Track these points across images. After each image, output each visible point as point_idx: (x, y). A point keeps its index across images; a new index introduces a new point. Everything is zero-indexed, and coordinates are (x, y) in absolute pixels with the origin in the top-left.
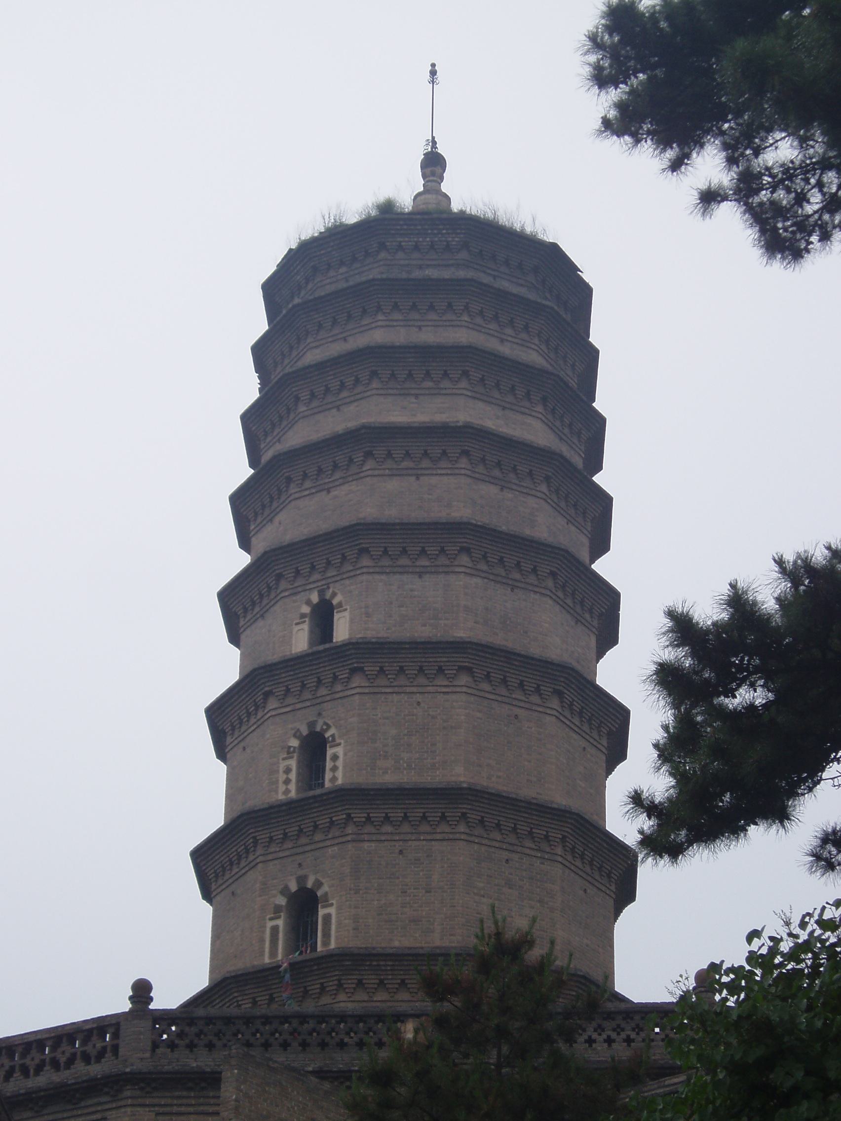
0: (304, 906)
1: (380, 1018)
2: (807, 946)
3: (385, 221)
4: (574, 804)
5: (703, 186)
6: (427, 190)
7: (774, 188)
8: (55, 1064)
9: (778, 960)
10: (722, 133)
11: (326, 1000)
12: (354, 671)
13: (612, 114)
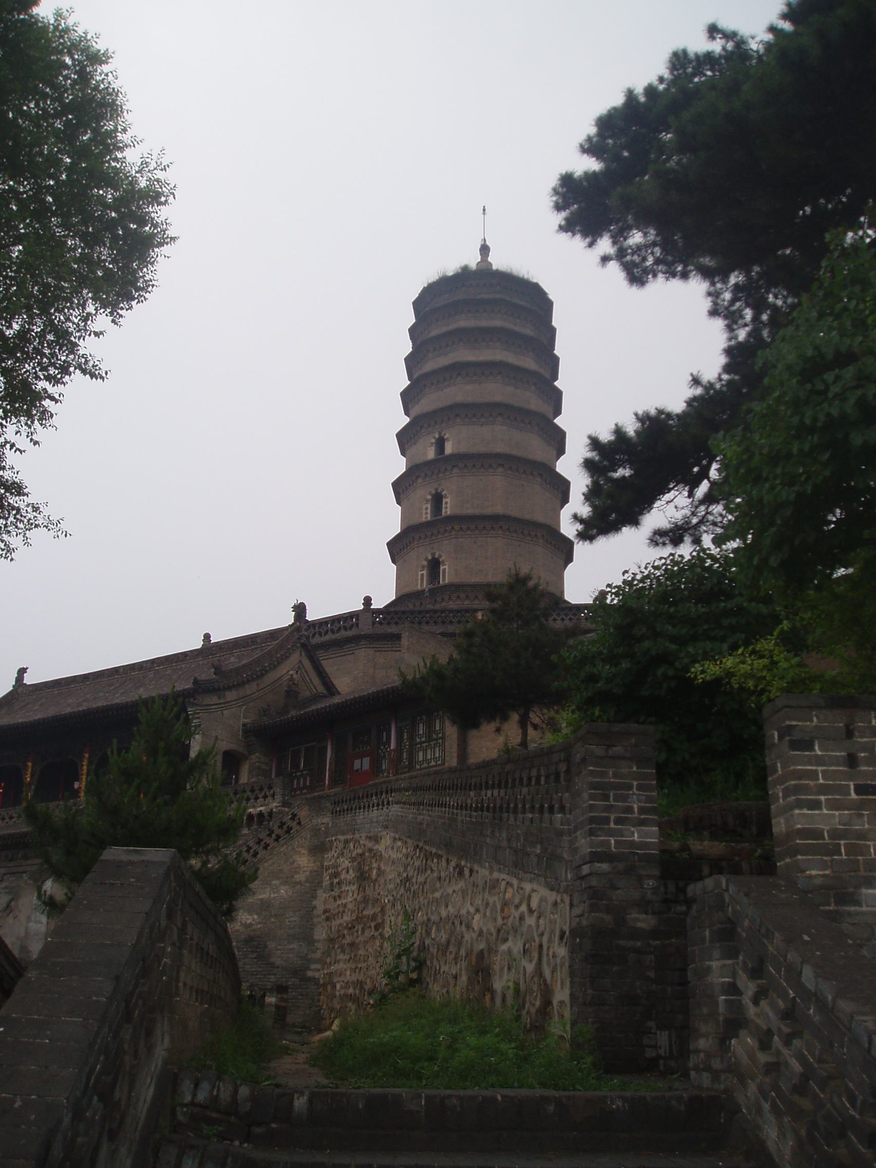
0: (434, 566)
1: (467, 611)
2: (648, 577)
3: (465, 274)
4: (548, 522)
5: (602, 254)
6: (482, 260)
7: (633, 254)
8: (333, 631)
9: (636, 582)
10: (610, 231)
11: (444, 604)
12: (454, 466)
13: (563, 223)
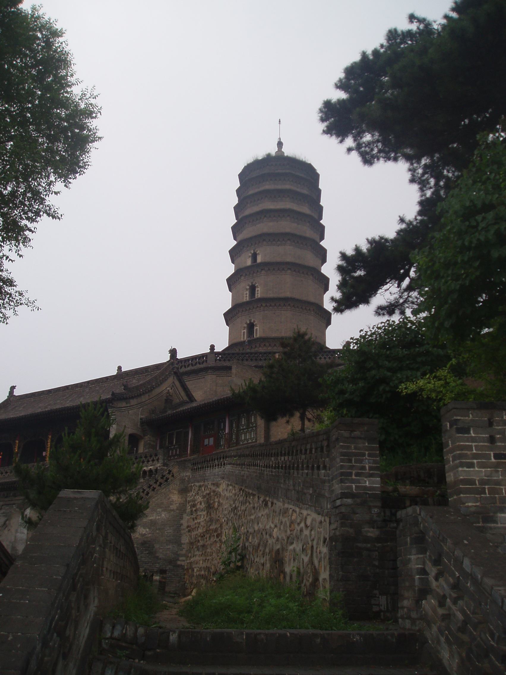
0: (251, 327)
1: (270, 353)
2: (374, 333)
3: (268, 158)
4: (317, 301)
5: (348, 147)
6: (278, 151)
7: (365, 147)
8: (192, 365)
9: (367, 337)
10: (353, 133)
11: (256, 349)
12: (262, 270)
13: (325, 129)
